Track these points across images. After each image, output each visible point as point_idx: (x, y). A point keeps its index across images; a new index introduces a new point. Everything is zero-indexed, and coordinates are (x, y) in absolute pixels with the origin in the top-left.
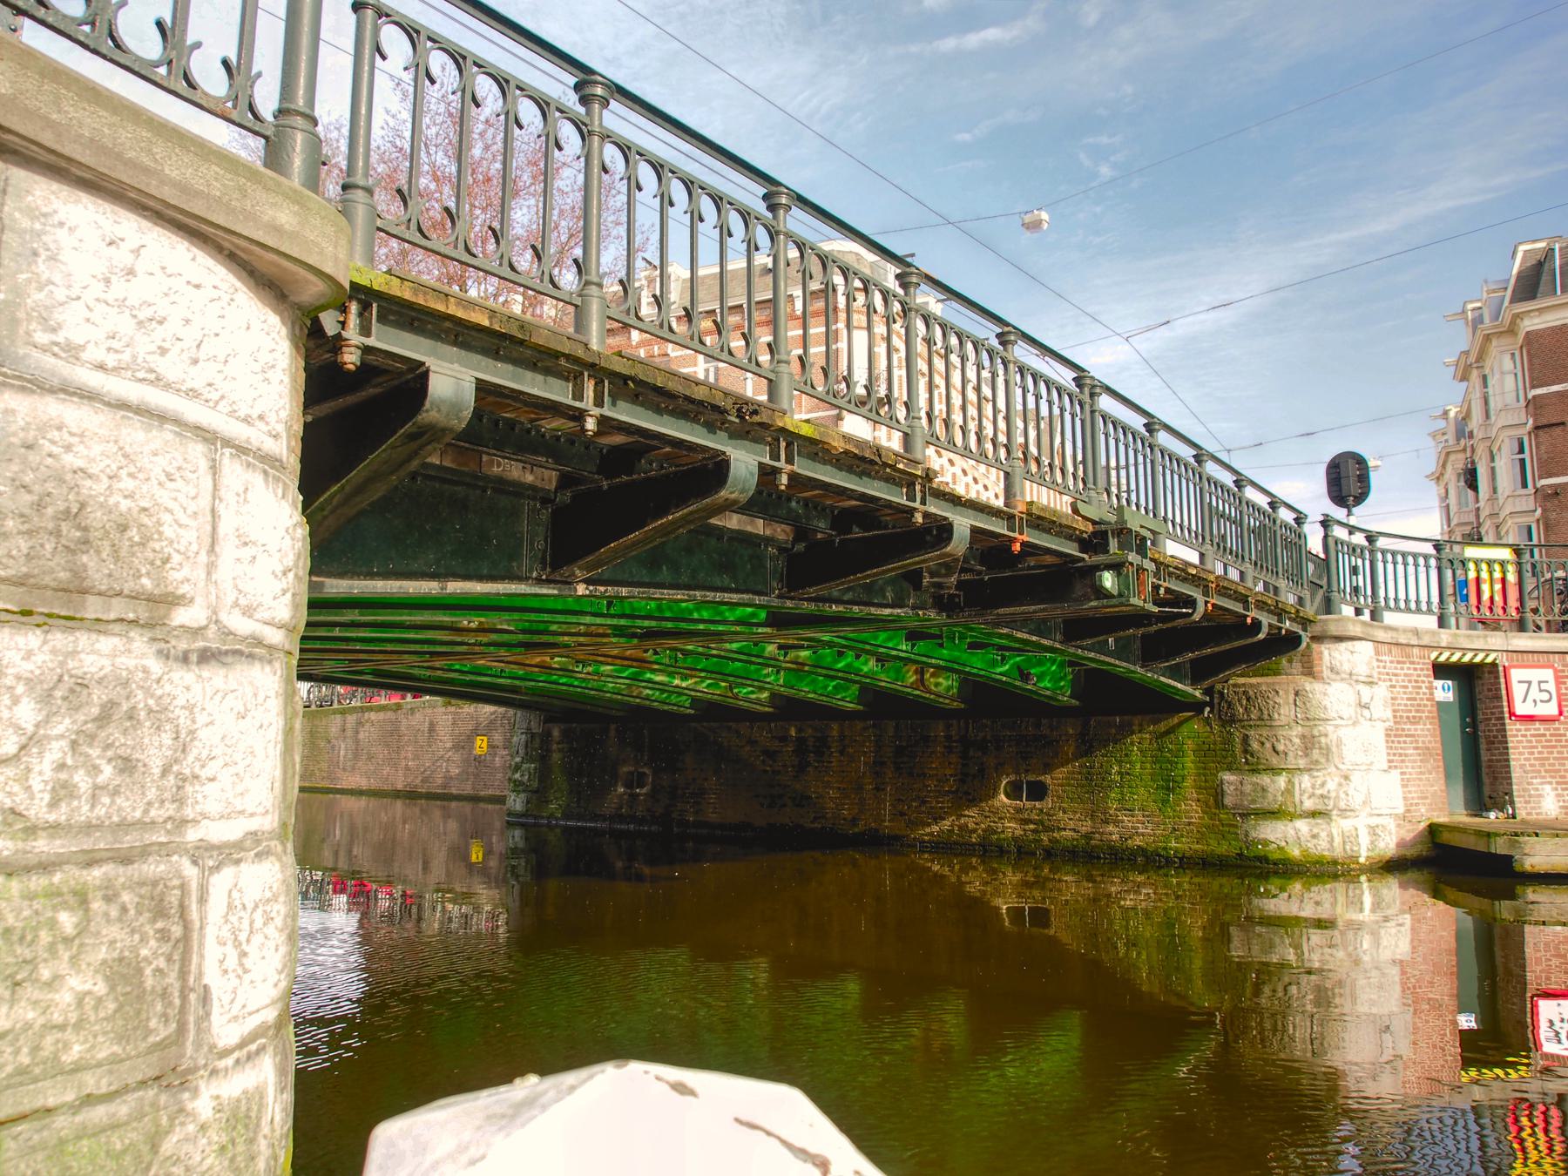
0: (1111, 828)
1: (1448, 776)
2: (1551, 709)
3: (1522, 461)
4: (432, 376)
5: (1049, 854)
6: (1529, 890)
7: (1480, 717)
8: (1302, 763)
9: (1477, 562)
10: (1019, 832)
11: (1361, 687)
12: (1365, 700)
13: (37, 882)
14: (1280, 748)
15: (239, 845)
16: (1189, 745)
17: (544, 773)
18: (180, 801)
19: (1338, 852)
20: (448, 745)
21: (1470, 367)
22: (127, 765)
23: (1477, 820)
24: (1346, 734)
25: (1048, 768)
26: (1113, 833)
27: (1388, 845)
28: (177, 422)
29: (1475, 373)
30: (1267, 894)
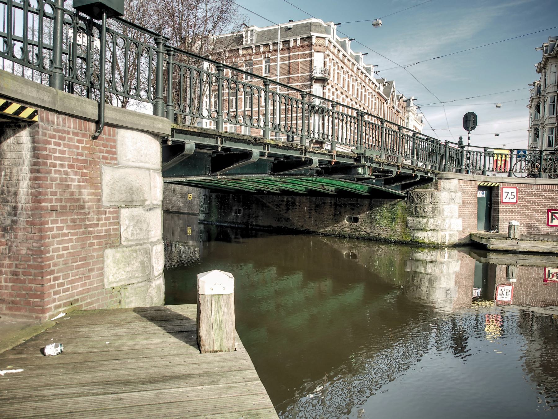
0: (376, 231)
1: (479, 219)
2: (514, 201)
3: (554, 105)
4: (186, 145)
5: (358, 238)
6: (491, 255)
7: (493, 202)
8: (431, 215)
9: (497, 154)
10: (350, 232)
11: (452, 193)
12: (453, 196)
13: (130, 249)
14: (426, 210)
15: (156, 242)
16: (400, 209)
17: (210, 209)
18: (148, 235)
19: (439, 241)
20: (180, 196)
21: (541, 69)
22: (141, 229)
23: (488, 233)
24: (446, 207)
25: (359, 213)
26: (376, 233)
27: (455, 240)
28: (144, 168)
29: (543, 71)
30: (418, 252)
